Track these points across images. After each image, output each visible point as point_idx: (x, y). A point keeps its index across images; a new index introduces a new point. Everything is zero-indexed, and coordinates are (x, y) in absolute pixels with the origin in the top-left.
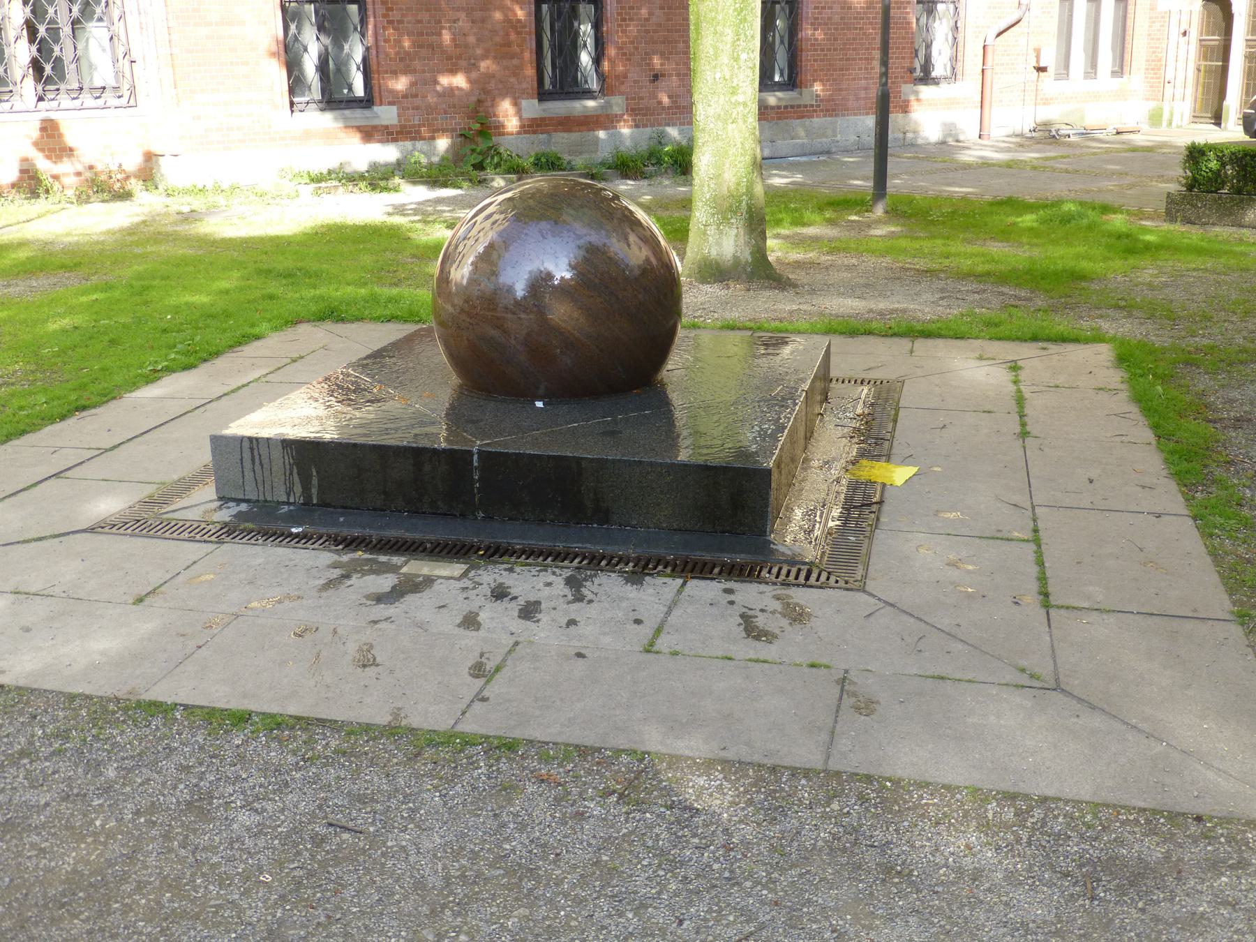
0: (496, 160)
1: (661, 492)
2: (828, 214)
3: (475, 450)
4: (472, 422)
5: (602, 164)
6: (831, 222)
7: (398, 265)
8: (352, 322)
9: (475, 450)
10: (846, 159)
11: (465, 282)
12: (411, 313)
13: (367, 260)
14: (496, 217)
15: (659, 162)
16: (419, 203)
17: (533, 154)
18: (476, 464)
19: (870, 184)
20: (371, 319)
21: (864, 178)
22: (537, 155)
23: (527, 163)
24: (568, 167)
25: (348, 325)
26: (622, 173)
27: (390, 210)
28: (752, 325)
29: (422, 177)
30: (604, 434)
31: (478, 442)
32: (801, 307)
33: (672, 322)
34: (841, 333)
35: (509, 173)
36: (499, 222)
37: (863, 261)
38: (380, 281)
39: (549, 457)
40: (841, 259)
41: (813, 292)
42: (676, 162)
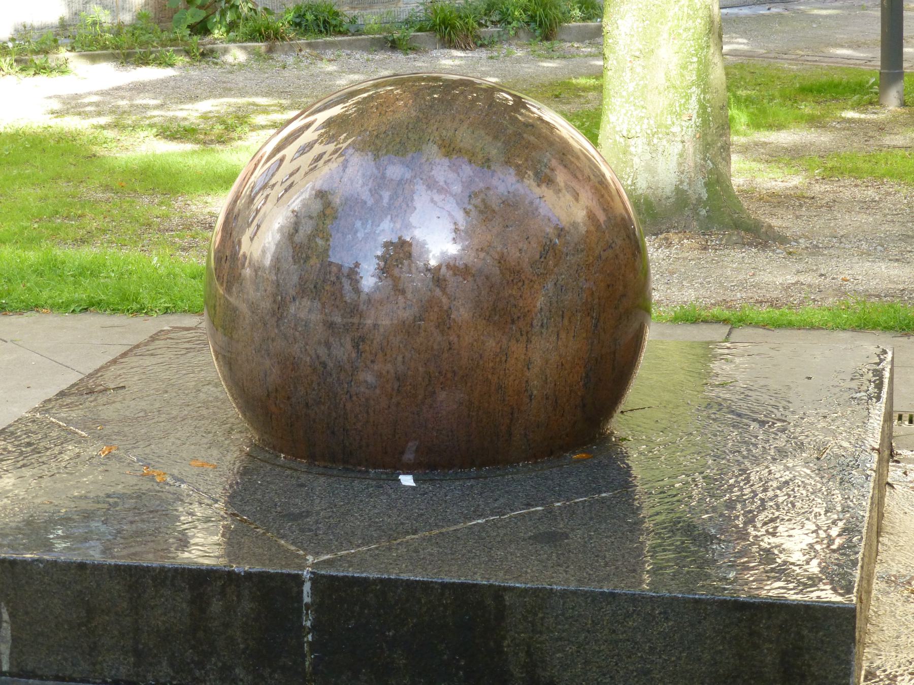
0: (229, 17)
1: (652, 650)
2: (807, 108)
3: (306, 574)
4: (293, 517)
5: (408, 23)
6: (814, 122)
7: (83, 207)
8: (19, 311)
9: (306, 574)
10: (816, 12)
11: (268, 262)
12: (125, 298)
13: (29, 195)
14: (318, 149)
15: (505, 20)
16: (102, 93)
17: (291, 6)
18: (307, 599)
19: (877, 53)
20: (52, 307)
21: (855, 45)
22: (298, 8)
23: (283, 21)
24: (352, 30)
25: (14, 319)
26: (443, 38)
27: (57, 105)
28: (727, 314)
29: (105, 47)
30: (536, 538)
31: (310, 558)
32: (802, 278)
33: (636, 325)
34: (887, 328)
35: (253, 39)
36: (325, 157)
37: (889, 194)
38: (55, 236)
39: (444, 585)
40: (848, 190)
41: (815, 250)
42: (533, 18)
